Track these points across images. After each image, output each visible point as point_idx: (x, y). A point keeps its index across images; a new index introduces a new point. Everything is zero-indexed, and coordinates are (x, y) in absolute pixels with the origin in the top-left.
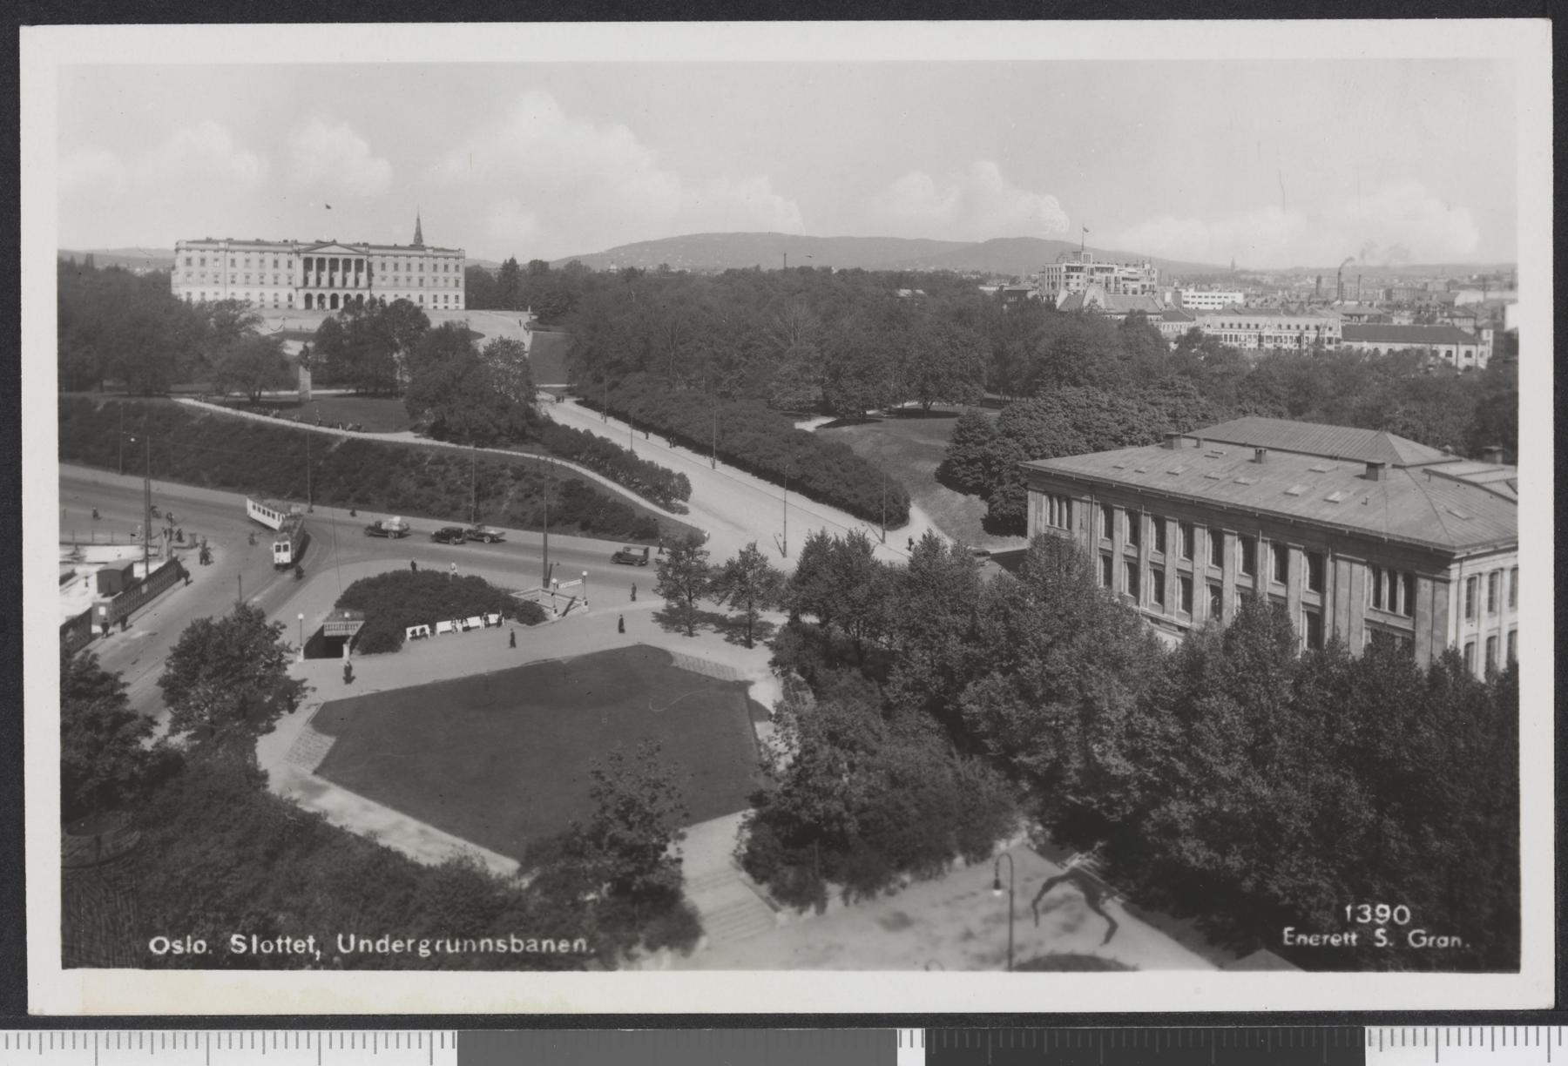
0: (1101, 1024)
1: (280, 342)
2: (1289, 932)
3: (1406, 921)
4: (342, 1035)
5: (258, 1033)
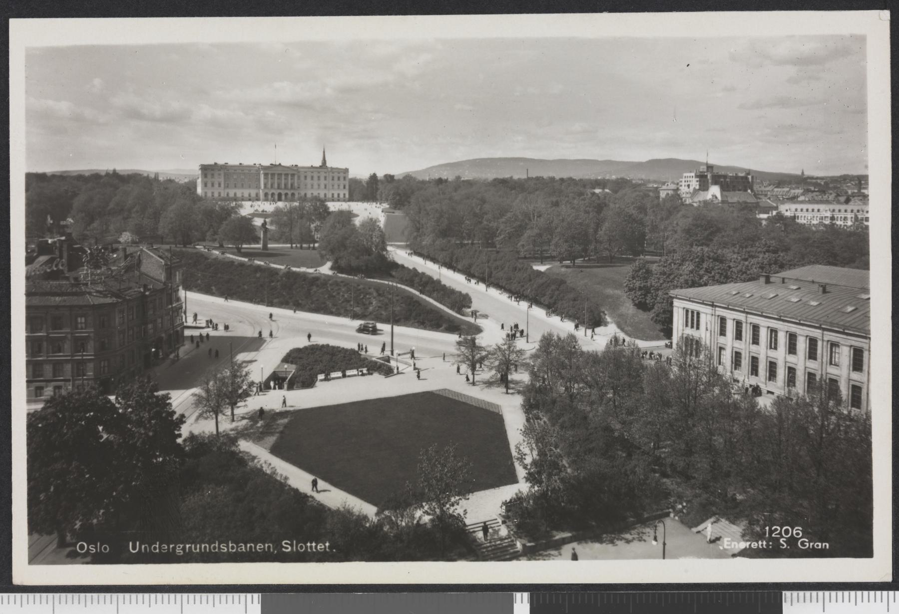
0: (631, 590)
1: (252, 218)
2: (728, 541)
4: (195, 596)
5: (146, 595)
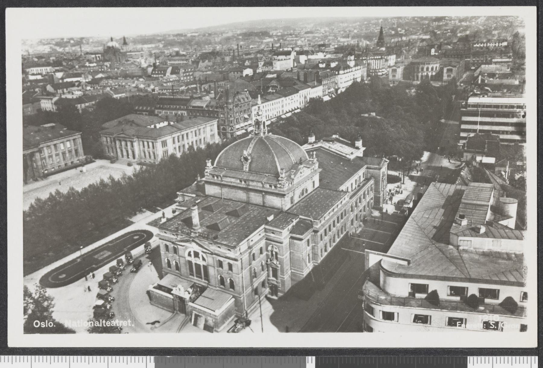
3: (36, 321)
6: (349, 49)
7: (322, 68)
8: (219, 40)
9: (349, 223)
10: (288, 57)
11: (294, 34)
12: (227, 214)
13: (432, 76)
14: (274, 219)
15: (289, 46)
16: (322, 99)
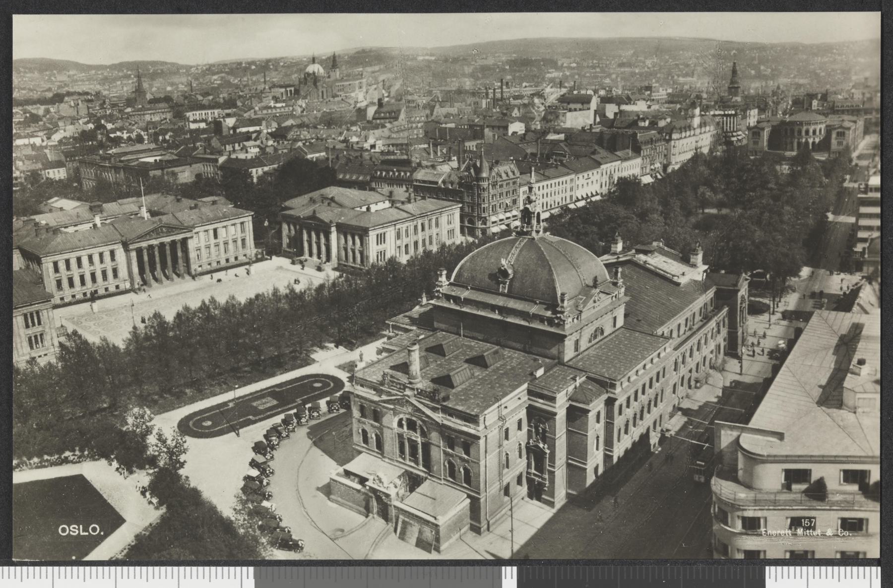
6: (692, 97)
7: (644, 128)
8: (470, 71)
9: (669, 390)
10: (586, 106)
11: (599, 66)
12: (467, 361)
13: (814, 143)
14: (545, 373)
15: (588, 87)
16: (640, 181)
